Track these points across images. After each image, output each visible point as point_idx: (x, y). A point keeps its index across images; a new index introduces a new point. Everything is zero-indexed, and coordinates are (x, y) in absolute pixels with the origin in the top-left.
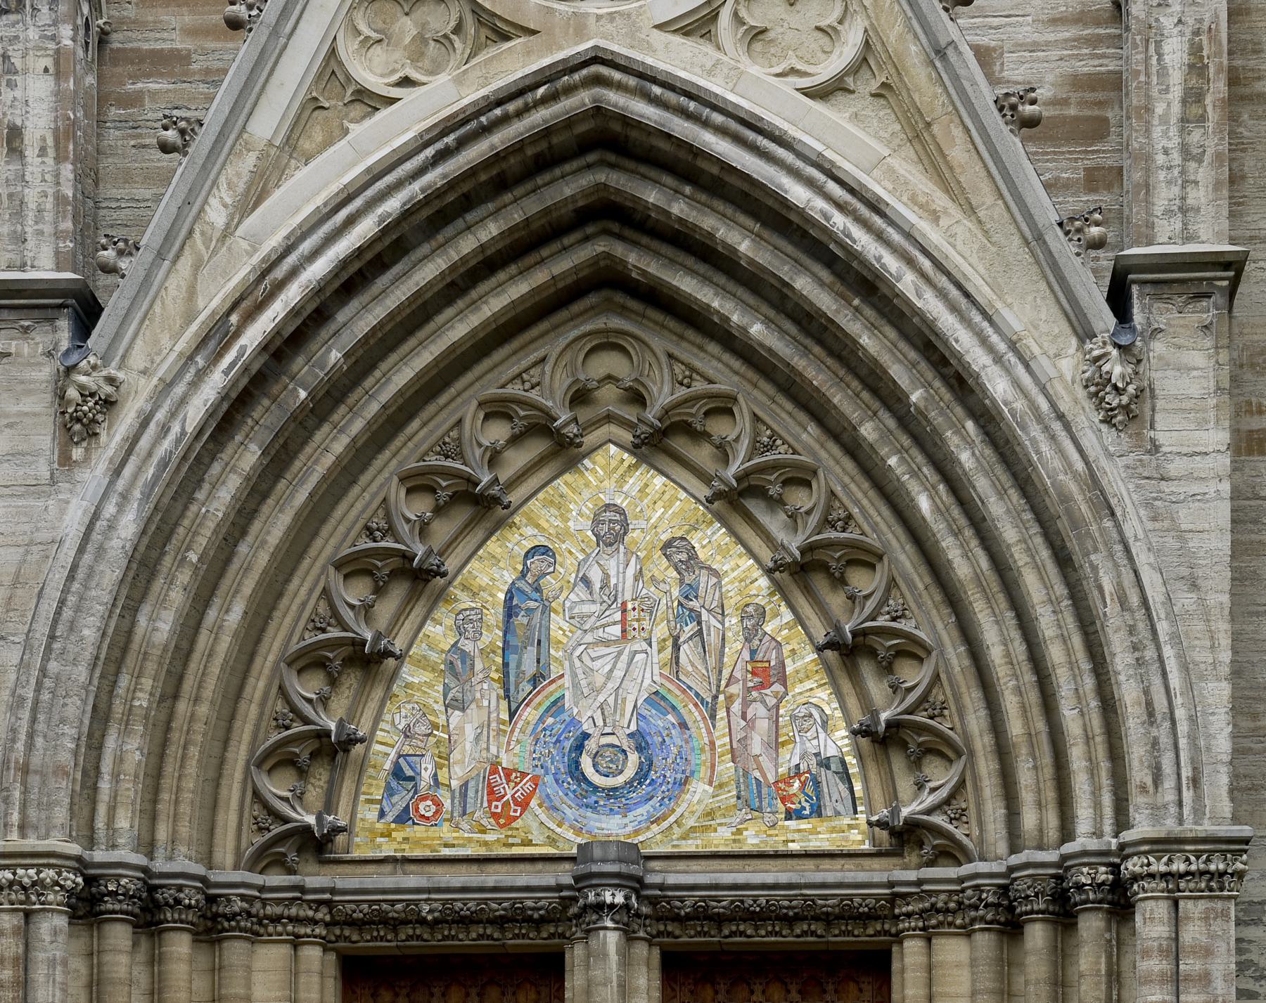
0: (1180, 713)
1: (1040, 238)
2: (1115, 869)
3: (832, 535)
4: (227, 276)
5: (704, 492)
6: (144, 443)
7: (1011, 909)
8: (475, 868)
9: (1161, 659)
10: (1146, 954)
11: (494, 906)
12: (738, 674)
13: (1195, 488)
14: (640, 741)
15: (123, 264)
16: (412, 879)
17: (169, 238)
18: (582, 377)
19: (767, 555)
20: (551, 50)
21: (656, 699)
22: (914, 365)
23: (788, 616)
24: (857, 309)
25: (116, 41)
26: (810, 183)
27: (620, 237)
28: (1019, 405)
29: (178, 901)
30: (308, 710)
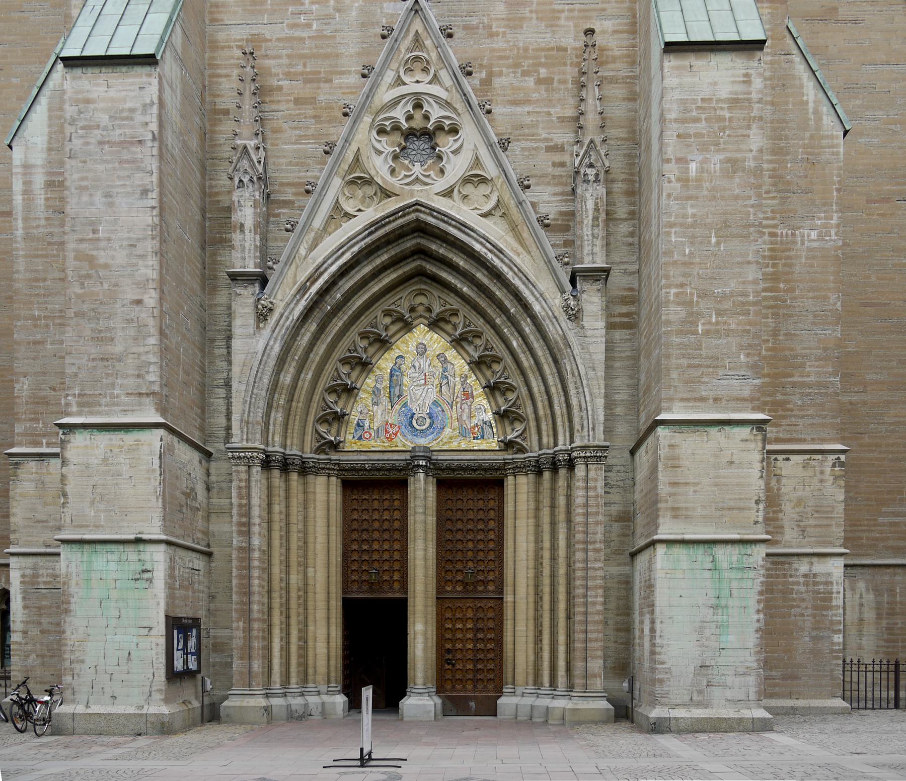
0: (589, 408)
1: (550, 262)
3: (488, 353)
4: (306, 270)
5: (449, 339)
6: (281, 322)
10: (578, 480)
13: (594, 340)
14: (430, 415)
15: (275, 267)
16: (363, 457)
17: (288, 258)
19: (468, 359)
21: (435, 403)
23: (474, 378)
25: (272, 197)
26: (481, 243)
27: (424, 260)
28: (543, 314)
30: (331, 405)
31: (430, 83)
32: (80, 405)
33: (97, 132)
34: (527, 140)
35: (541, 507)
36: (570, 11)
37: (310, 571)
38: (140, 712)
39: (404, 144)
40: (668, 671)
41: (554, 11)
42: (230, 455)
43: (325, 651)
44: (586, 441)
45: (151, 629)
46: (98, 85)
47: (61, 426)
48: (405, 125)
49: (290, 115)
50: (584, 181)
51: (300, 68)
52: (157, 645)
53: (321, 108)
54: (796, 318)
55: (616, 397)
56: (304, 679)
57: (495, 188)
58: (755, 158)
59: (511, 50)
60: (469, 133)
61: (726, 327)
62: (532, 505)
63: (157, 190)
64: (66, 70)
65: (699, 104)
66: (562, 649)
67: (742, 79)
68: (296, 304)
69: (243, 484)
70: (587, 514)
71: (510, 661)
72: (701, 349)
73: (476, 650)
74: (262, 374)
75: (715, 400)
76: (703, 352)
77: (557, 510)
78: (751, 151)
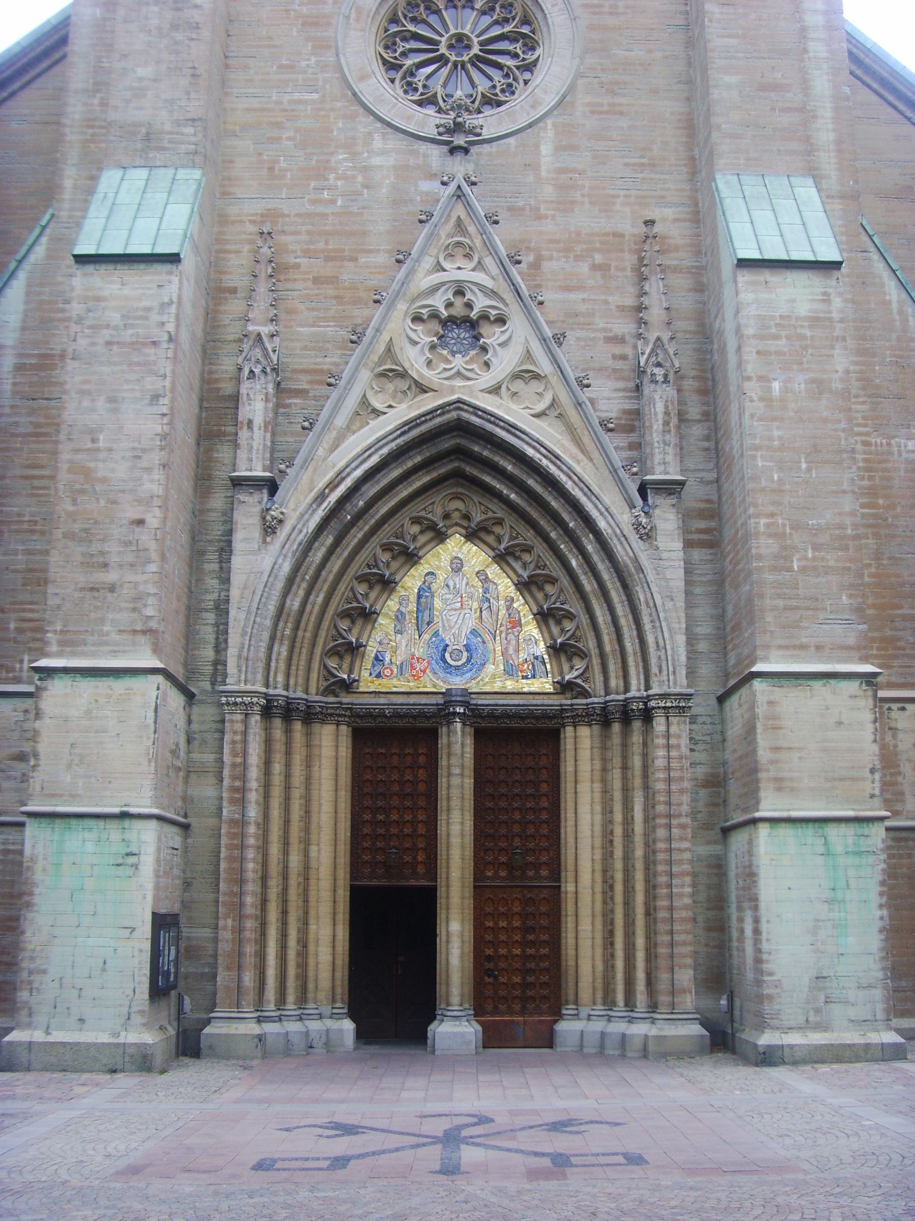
0: (668, 647)
1: (615, 471)
2: (645, 704)
3: (540, 572)
5: (492, 554)
6: (293, 536)
7: (606, 716)
9: (661, 627)
10: (658, 737)
12: (504, 623)
14: (468, 648)
15: (288, 471)
16: (382, 700)
17: (305, 462)
19: (515, 579)
20: (442, 398)
21: (474, 632)
22: (570, 513)
23: (522, 601)
26: (534, 448)
27: (463, 461)
28: (609, 531)
29: (298, 709)
31: (473, 270)
32: (61, 643)
33: (105, 332)
34: (582, 329)
35: (609, 766)
36: (626, 196)
37: (313, 849)
38: (115, 1041)
39: (442, 332)
40: (778, 984)
42: (224, 700)
43: (330, 958)
45: (133, 929)
47: (37, 670)
48: (444, 313)
49: (308, 295)
50: (652, 381)
51: (321, 245)
52: (141, 951)
53: (344, 288)
54: (900, 539)
56: (303, 998)
57: (549, 386)
58: (842, 380)
60: (518, 325)
61: (824, 564)
62: (598, 765)
63: (169, 395)
64: (77, 266)
66: (640, 956)
67: (821, 298)
68: (312, 515)
69: (238, 738)
70: (669, 780)
71: (571, 971)
72: (798, 589)
73: (525, 958)
74: (267, 598)
75: (818, 648)
76: (801, 592)
77: (630, 772)
78: (837, 372)
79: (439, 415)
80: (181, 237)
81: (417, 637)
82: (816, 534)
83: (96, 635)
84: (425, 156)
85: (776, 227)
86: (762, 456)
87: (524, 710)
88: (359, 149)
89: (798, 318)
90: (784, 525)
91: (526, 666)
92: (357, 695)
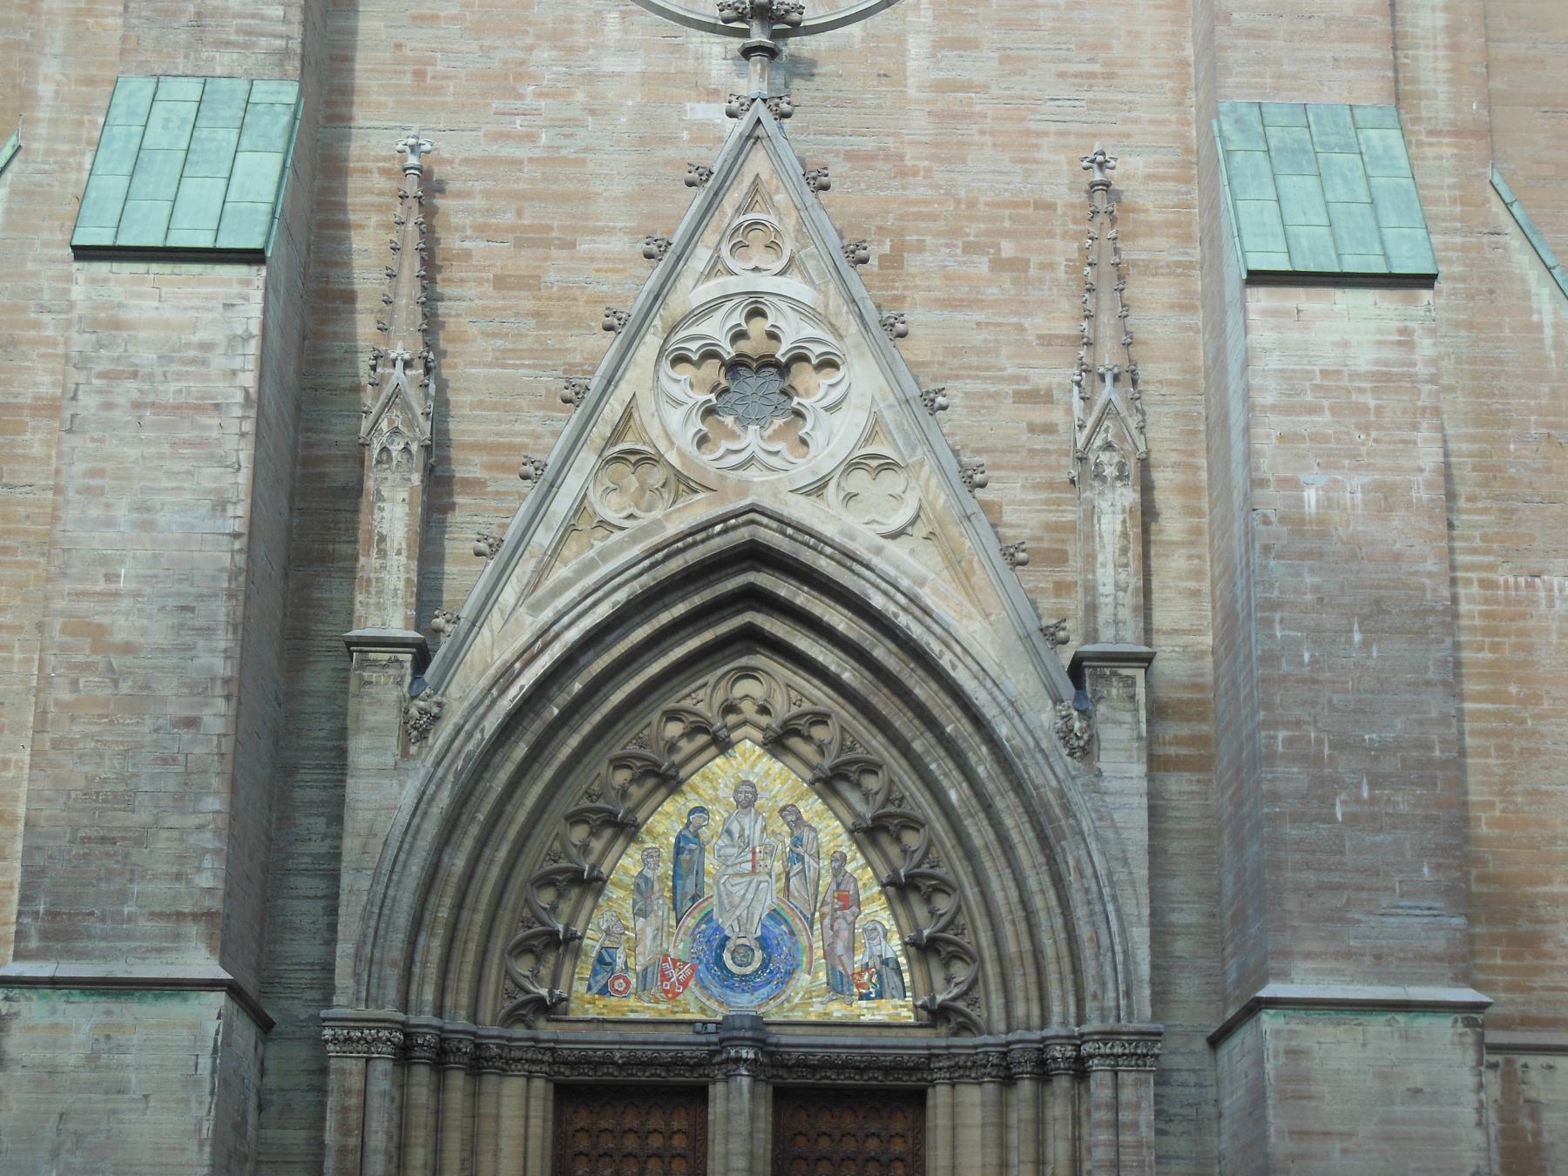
0: (1118, 948)
5: (809, 775)
7: (1008, 1068)
8: (651, 1027)
9: (1105, 911)
11: (664, 1055)
12: (828, 899)
13: (1125, 800)
14: (763, 942)
16: (610, 1034)
18: (730, 696)
21: (774, 915)
23: (862, 861)
24: (912, 670)
29: (459, 1050)
30: (544, 916)
32: (45, 935)
33: (131, 384)
34: (976, 377)
36: (1060, 134)
41: (1028, 133)
42: (328, 1033)
44: (1112, 1021)
46: (141, 295)
49: (485, 308)
51: (509, 218)
53: (550, 298)
55: (1174, 918)
59: (941, 203)
65: (1318, 381)
67: (1396, 338)
69: (353, 1101)
72: (1342, 853)
75: (1378, 957)
78: (1421, 470)
79: (720, 533)
80: (267, 218)
81: (673, 923)
82: (1376, 758)
83: (109, 922)
84: (699, 57)
85: (1322, 209)
86: (1282, 620)
87: (862, 1055)
88: (580, 41)
89: (1354, 376)
90: (1319, 742)
91: (866, 976)
92: (566, 1025)
